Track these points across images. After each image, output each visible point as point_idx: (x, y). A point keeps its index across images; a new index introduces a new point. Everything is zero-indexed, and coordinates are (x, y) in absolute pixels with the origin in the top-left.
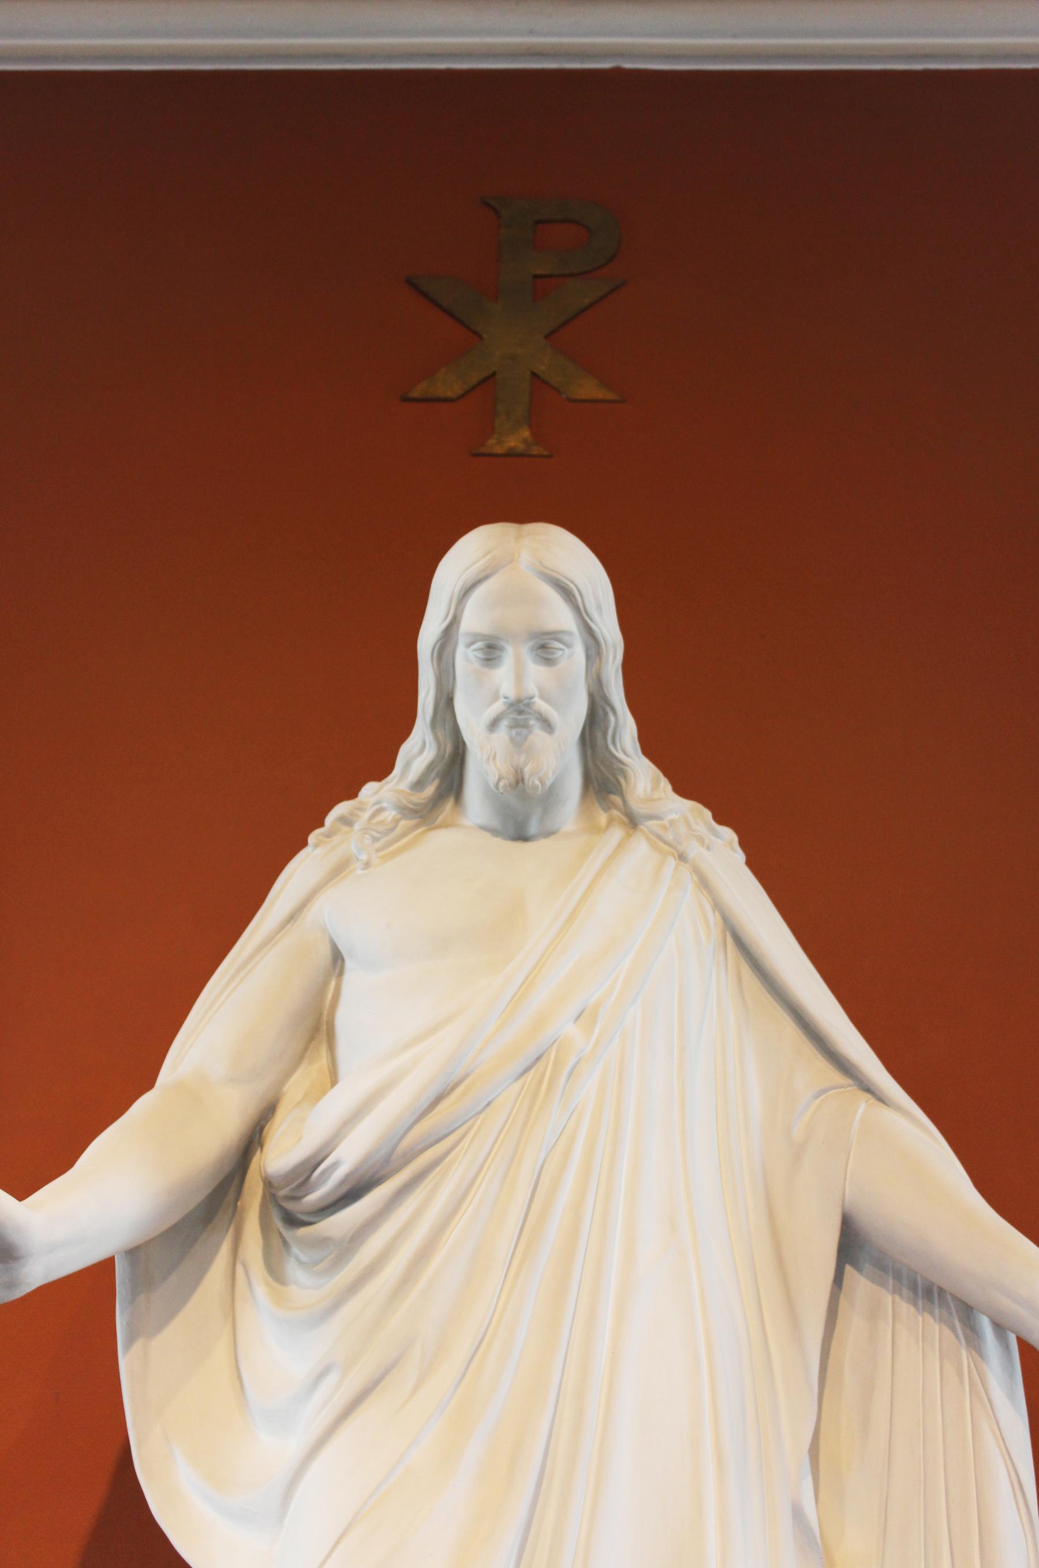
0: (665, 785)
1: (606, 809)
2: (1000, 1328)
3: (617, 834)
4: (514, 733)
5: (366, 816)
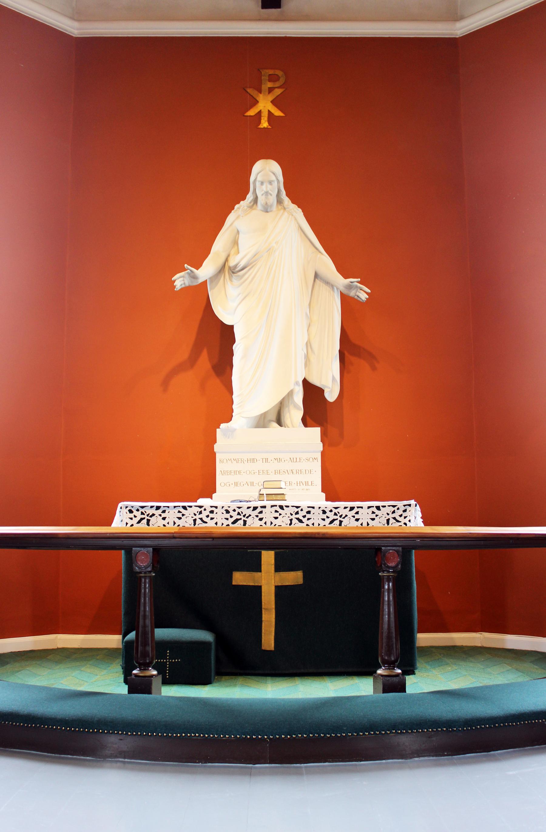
0: (290, 202)
2: (337, 289)
3: (282, 211)
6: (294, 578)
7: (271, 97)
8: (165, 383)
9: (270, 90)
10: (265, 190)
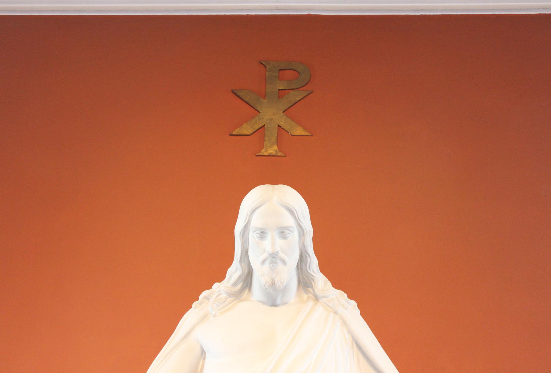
0: (329, 284)
1: (307, 293)
3: (311, 303)
4: (271, 265)
5: (215, 296)
7: (284, 104)
9: (282, 93)
10: (269, 249)
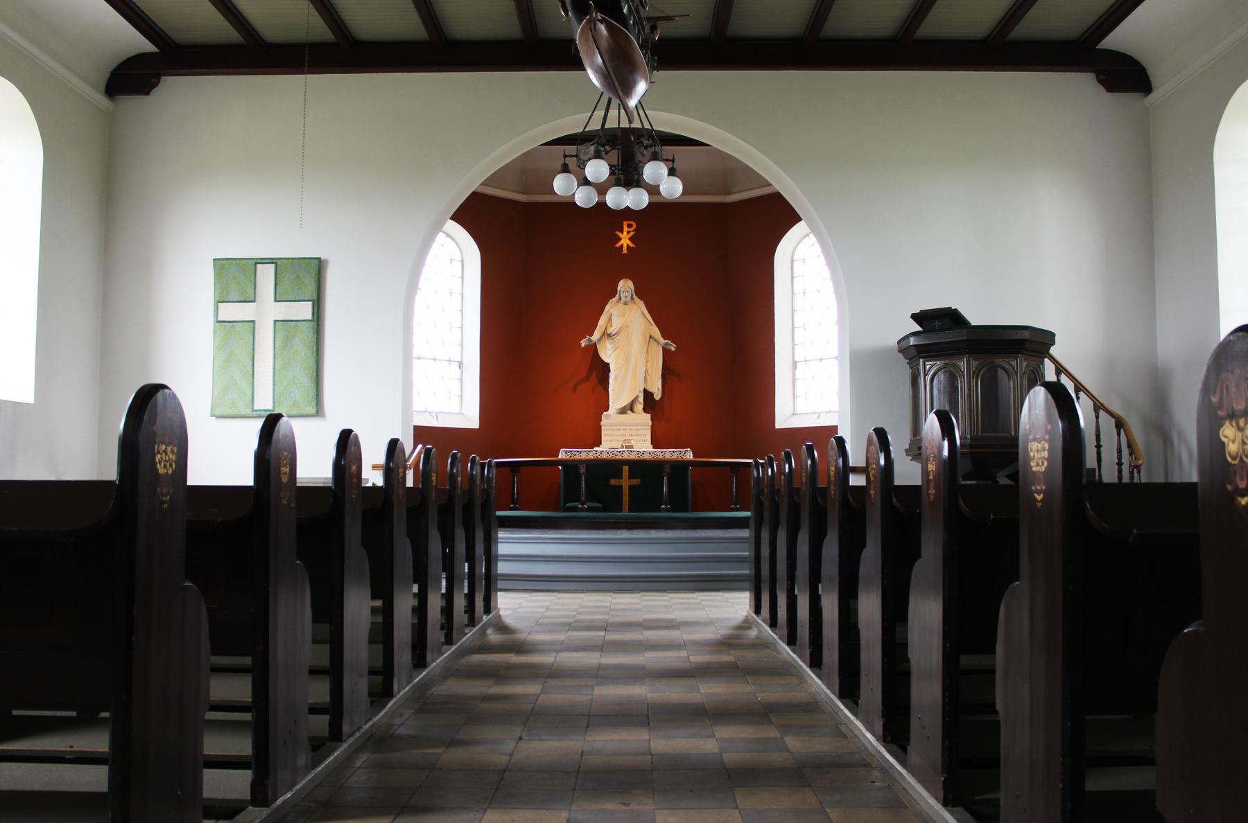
6: (636, 482)
8: (574, 389)
